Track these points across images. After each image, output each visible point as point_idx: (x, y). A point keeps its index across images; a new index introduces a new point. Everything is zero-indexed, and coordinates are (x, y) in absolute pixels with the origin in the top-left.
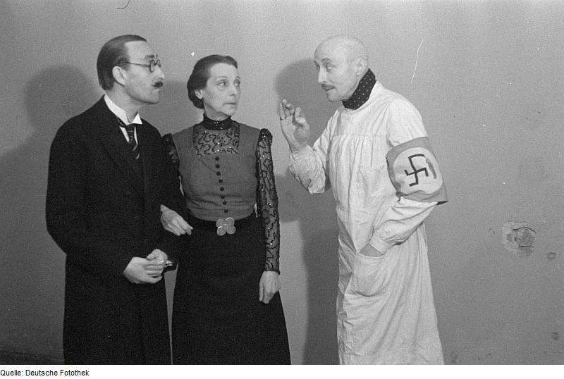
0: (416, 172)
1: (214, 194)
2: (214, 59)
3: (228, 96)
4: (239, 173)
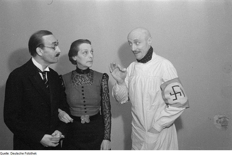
0: (175, 94)
1: (81, 104)
2: (80, 41)
3: (88, 59)
4: (93, 94)
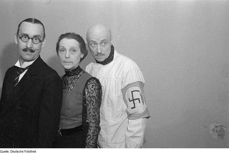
0: (133, 100)
